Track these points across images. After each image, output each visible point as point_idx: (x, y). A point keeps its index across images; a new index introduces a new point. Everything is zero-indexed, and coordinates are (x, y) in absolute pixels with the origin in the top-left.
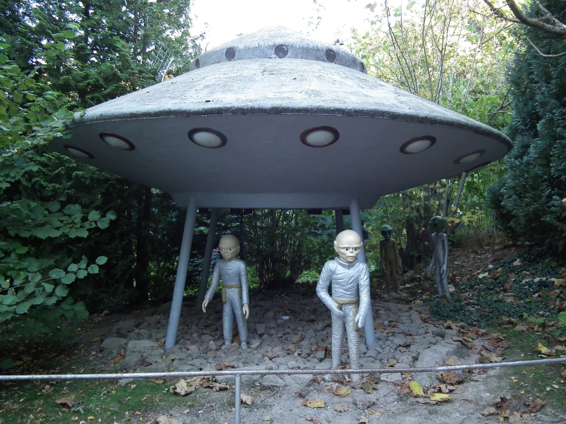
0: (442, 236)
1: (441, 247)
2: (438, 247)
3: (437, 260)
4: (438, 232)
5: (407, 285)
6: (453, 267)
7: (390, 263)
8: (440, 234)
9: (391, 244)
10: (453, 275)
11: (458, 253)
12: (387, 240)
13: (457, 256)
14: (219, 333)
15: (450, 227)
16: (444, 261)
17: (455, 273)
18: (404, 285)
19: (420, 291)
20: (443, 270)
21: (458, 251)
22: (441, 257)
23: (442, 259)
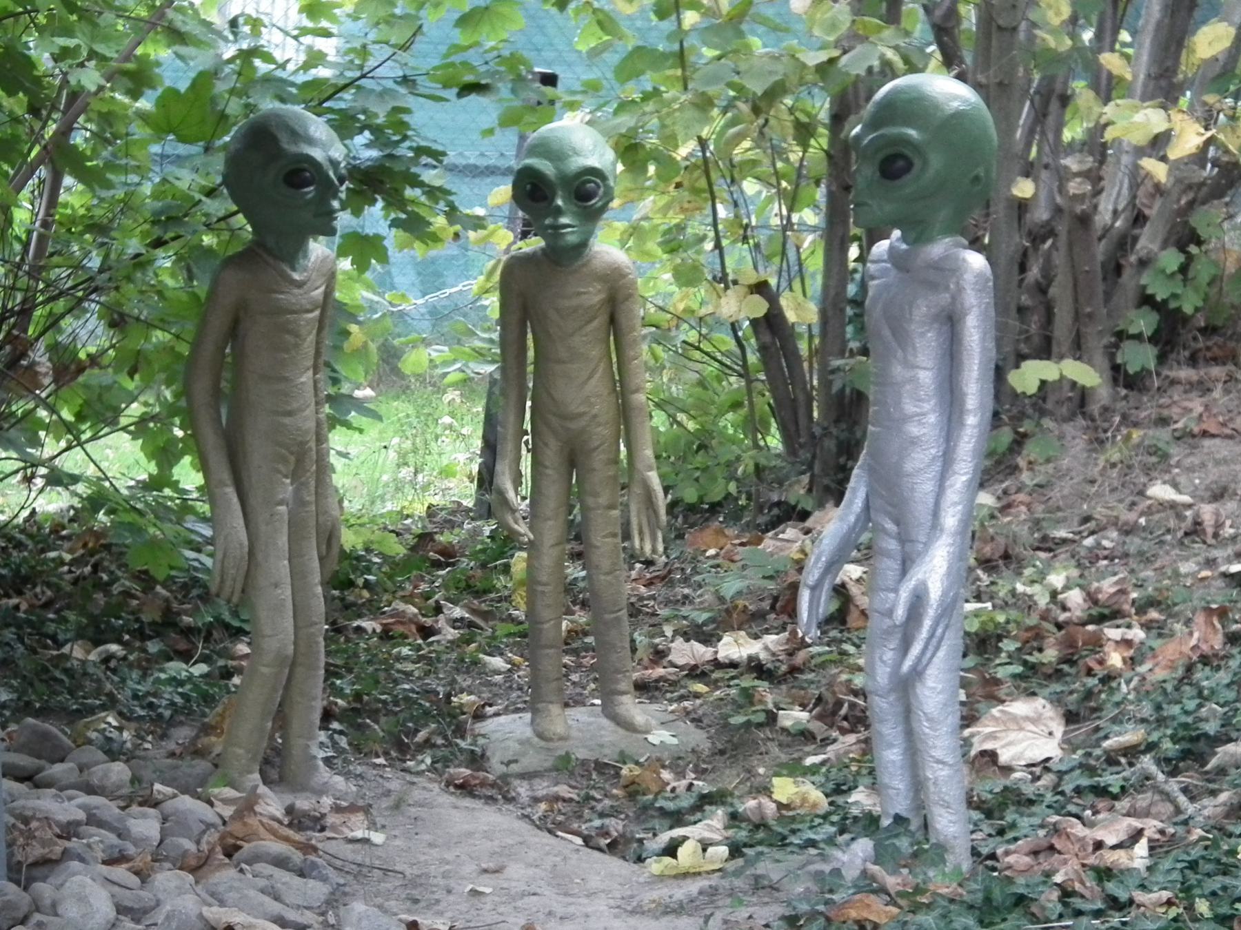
0: (947, 270)
1: (926, 377)
2: (898, 371)
3: (890, 495)
4: (917, 232)
5: (735, 647)
6: (1128, 530)
7: (574, 459)
8: (938, 248)
9: (594, 295)
10: (1092, 598)
11: (1197, 406)
12: (562, 257)
13: (1183, 436)
14: (840, 476)
15: (1158, 189)
16: (936, 513)
17: (1107, 586)
18: (708, 639)
19: (794, 717)
20: (918, 601)
21: (1202, 387)
22: (920, 463)
23: (925, 487)
